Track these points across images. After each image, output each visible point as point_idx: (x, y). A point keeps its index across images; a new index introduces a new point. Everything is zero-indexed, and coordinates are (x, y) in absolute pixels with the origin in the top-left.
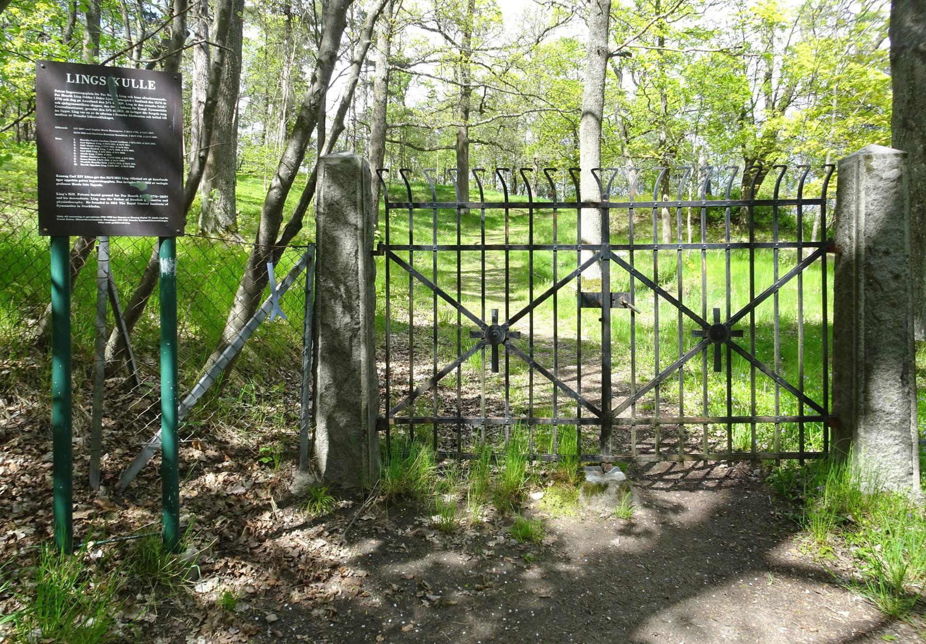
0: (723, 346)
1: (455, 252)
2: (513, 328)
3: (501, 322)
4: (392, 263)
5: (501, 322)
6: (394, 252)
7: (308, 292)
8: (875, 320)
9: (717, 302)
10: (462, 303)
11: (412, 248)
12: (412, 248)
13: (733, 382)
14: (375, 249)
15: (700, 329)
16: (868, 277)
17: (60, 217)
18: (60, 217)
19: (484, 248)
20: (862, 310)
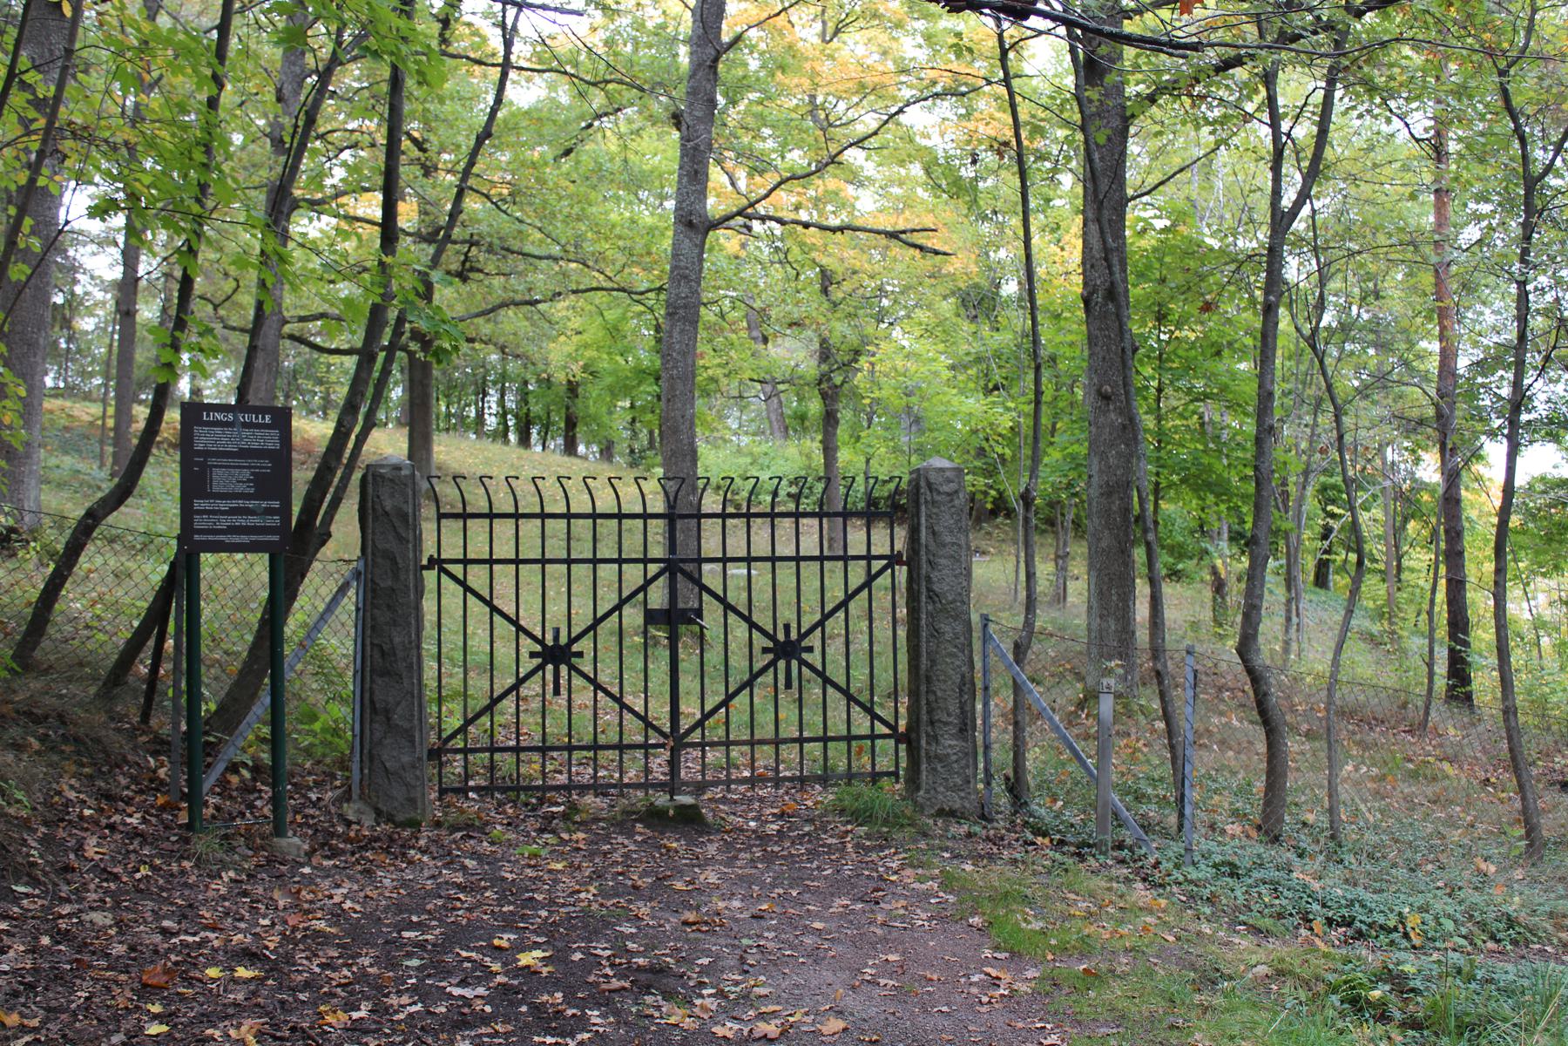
0: (795, 663)
1: (641, 566)
2: (575, 648)
3: (563, 640)
4: (444, 578)
5: (563, 640)
6: (209, 706)
7: (358, 609)
8: (936, 633)
9: (787, 614)
10: (495, 602)
11: (466, 562)
12: (466, 562)
13: (682, 656)
14: (425, 562)
15: (771, 645)
16: (929, 590)
17: (196, 537)
18: (196, 537)
19: (620, 561)
20: (923, 622)
